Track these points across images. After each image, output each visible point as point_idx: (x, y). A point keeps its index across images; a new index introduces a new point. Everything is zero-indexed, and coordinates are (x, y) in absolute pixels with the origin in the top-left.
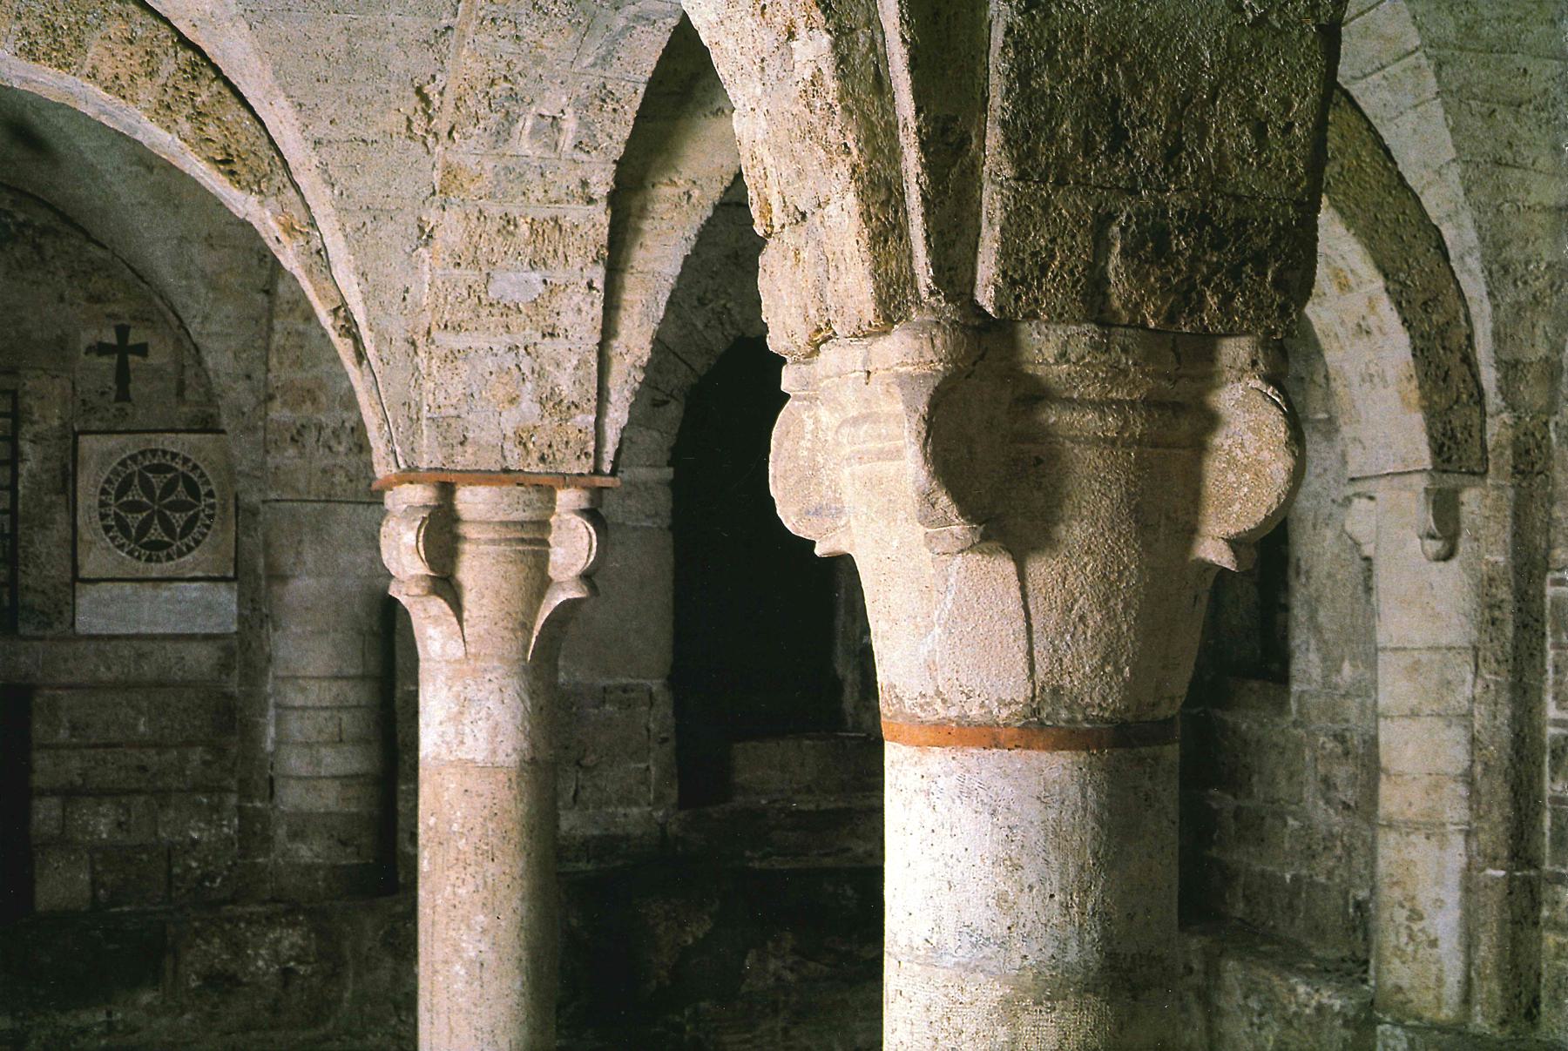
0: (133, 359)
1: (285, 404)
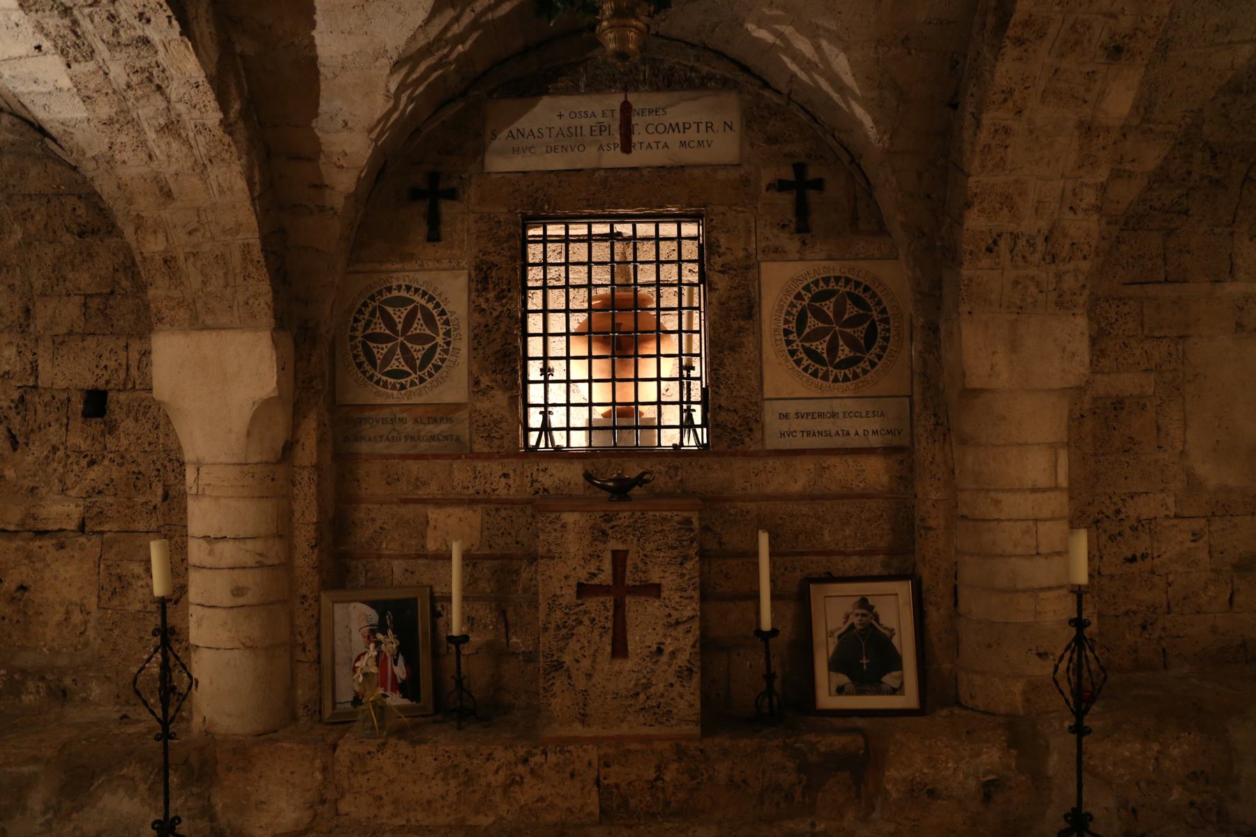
0: (812, 195)
1: (982, 211)
